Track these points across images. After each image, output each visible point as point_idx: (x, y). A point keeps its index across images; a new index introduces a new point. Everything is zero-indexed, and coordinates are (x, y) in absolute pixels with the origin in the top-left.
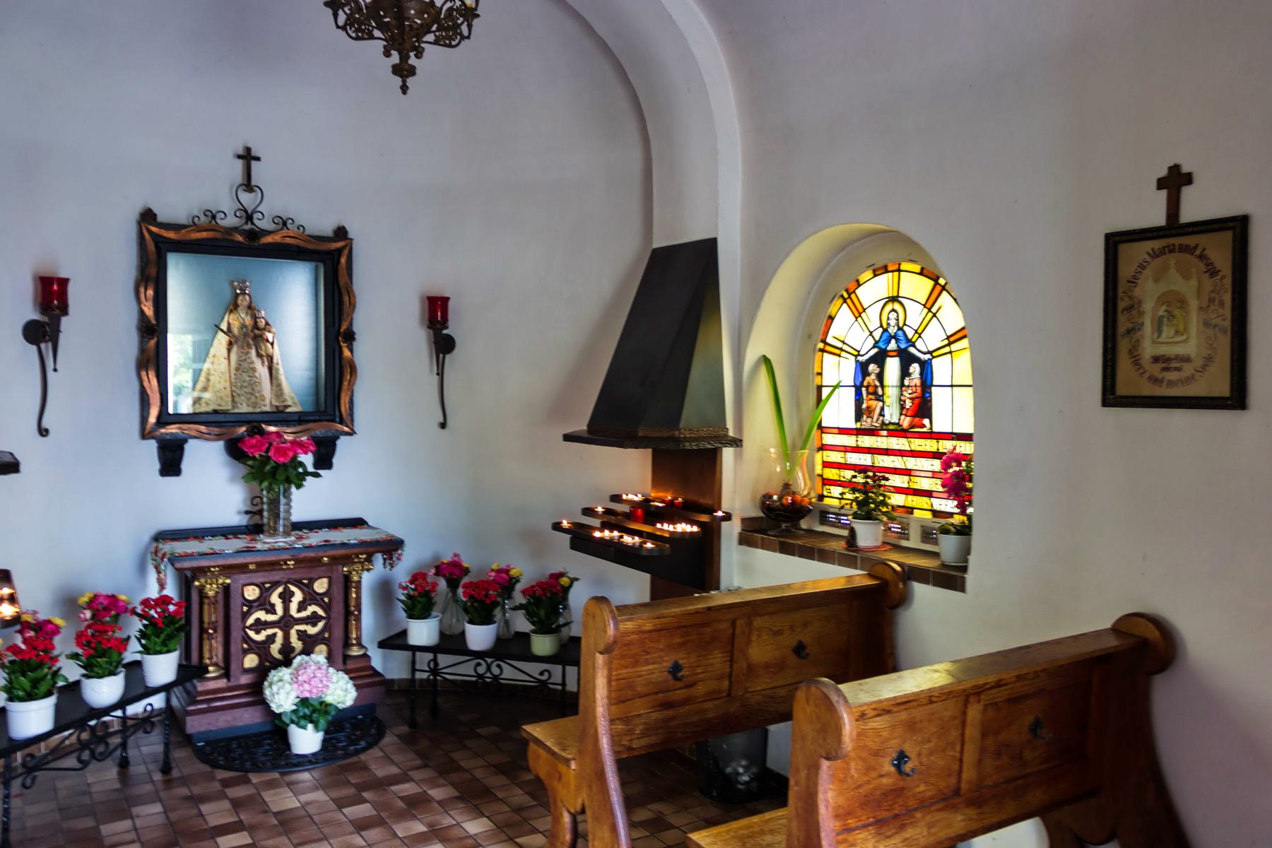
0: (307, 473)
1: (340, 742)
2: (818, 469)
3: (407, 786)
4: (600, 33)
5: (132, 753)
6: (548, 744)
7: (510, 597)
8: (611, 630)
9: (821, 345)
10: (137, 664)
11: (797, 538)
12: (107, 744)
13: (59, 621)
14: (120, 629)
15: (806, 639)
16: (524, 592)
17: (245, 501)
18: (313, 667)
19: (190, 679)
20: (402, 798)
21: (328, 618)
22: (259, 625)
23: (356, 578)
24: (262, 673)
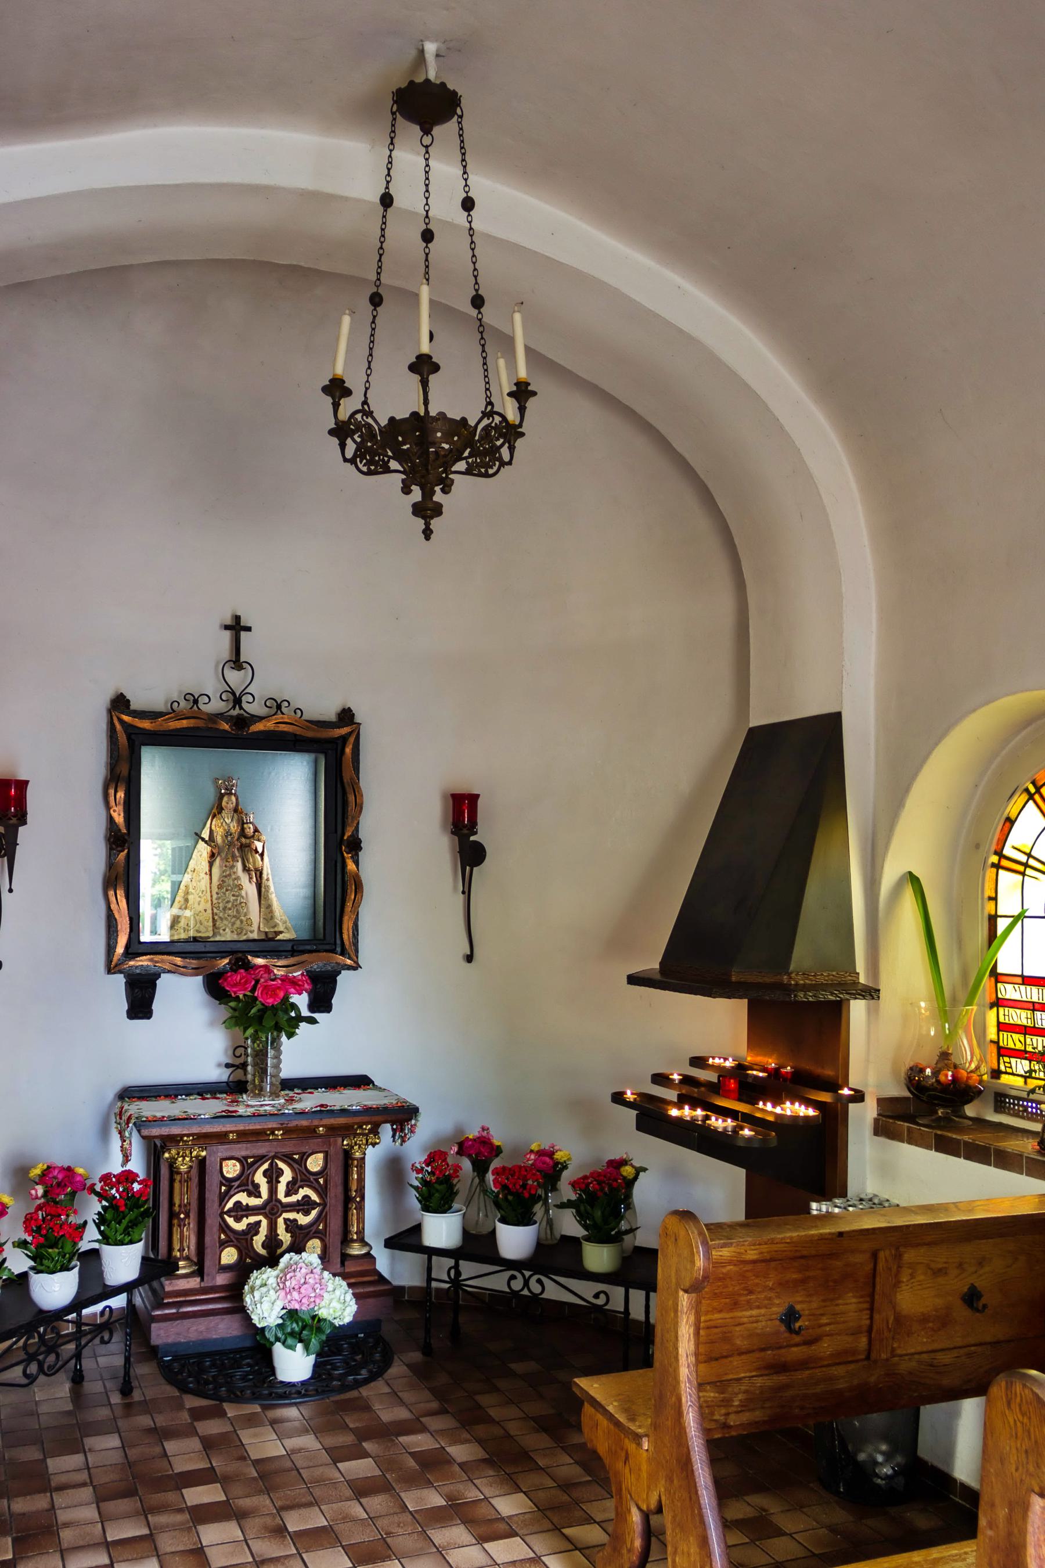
0: (300, 1019)
2: (992, 1033)
3: (419, 1437)
4: (679, 449)
5: (87, 1364)
6: (610, 1408)
7: (554, 1189)
8: (700, 1262)
9: (995, 859)
10: (94, 1254)
11: (961, 1130)
14: (75, 1212)
15: (980, 1283)
16: (574, 1184)
19: (158, 1277)
20: (413, 1455)
21: (324, 1204)
22: (240, 1211)
23: (358, 1155)
24: (242, 1271)
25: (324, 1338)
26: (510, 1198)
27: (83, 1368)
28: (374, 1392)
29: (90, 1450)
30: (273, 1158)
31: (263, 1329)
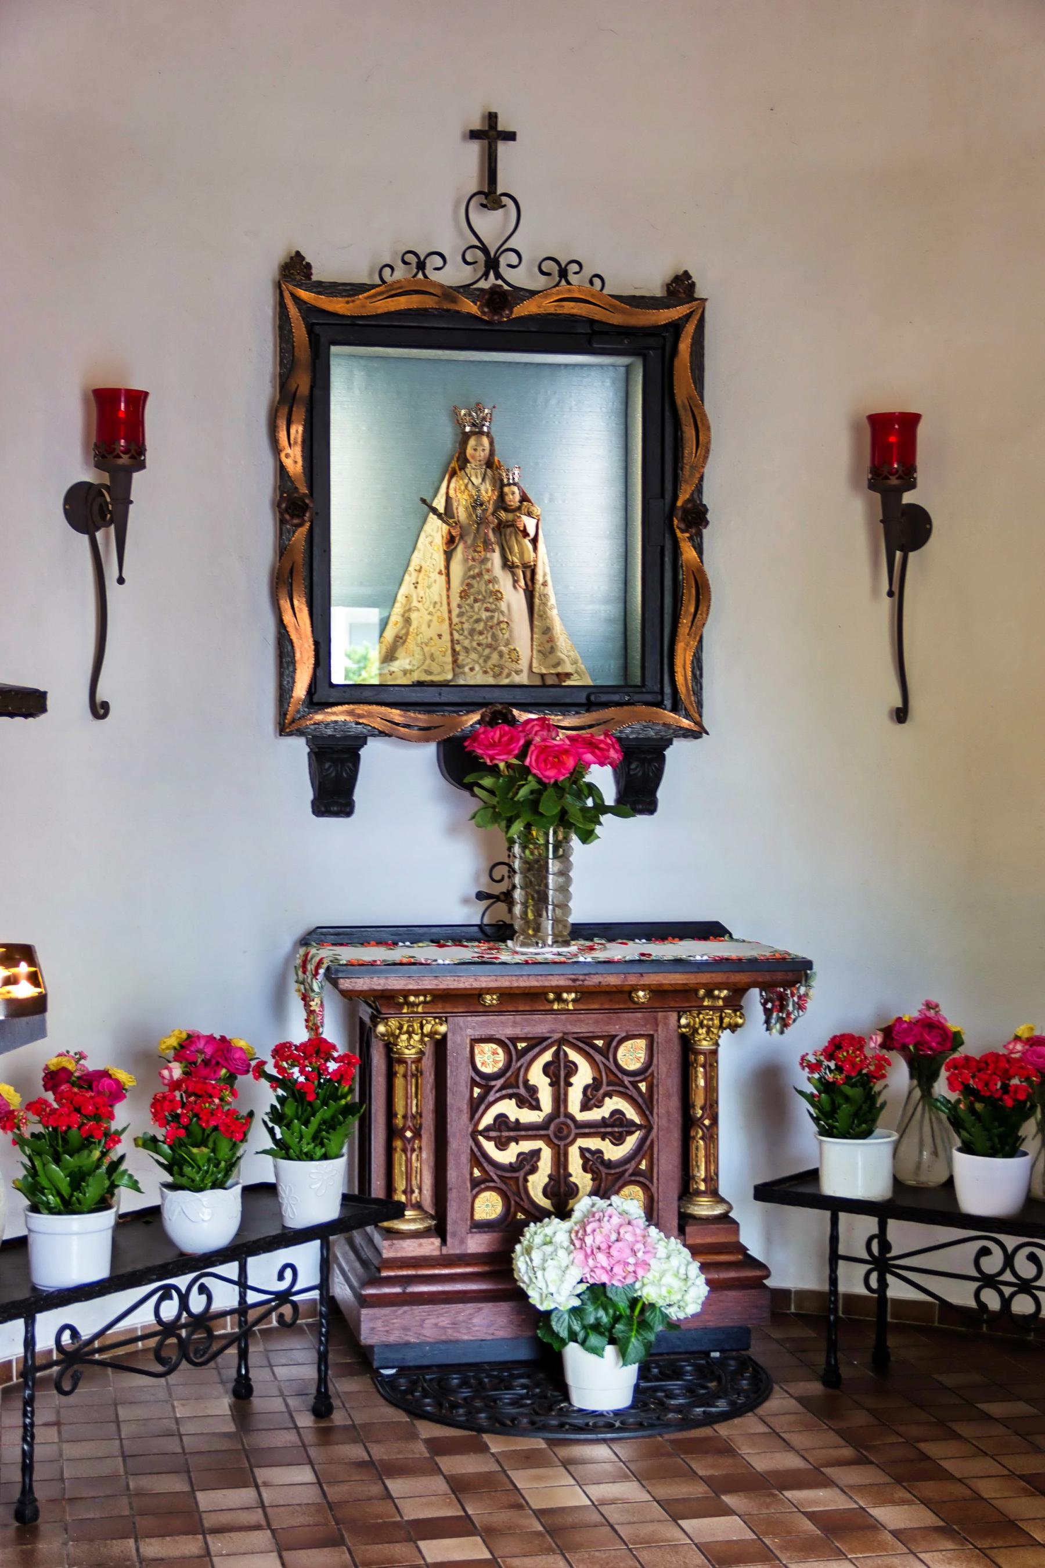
0: (601, 808)
1: (671, 1396)
3: (821, 1493)
5: (258, 1376)
12: (209, 1331)
13: (122, 1076)
17: (477, 877)
18: (616, 1220)
20: (811, 1516)
21: (648, 1127)
23: (705, 1045)
25: (652, 1337)
26: (979, 1106)
27: (251, 1375)
28: (742, 1433)
29: (265, 1484)
30: (562, 1041)
31: (548, 1314)
